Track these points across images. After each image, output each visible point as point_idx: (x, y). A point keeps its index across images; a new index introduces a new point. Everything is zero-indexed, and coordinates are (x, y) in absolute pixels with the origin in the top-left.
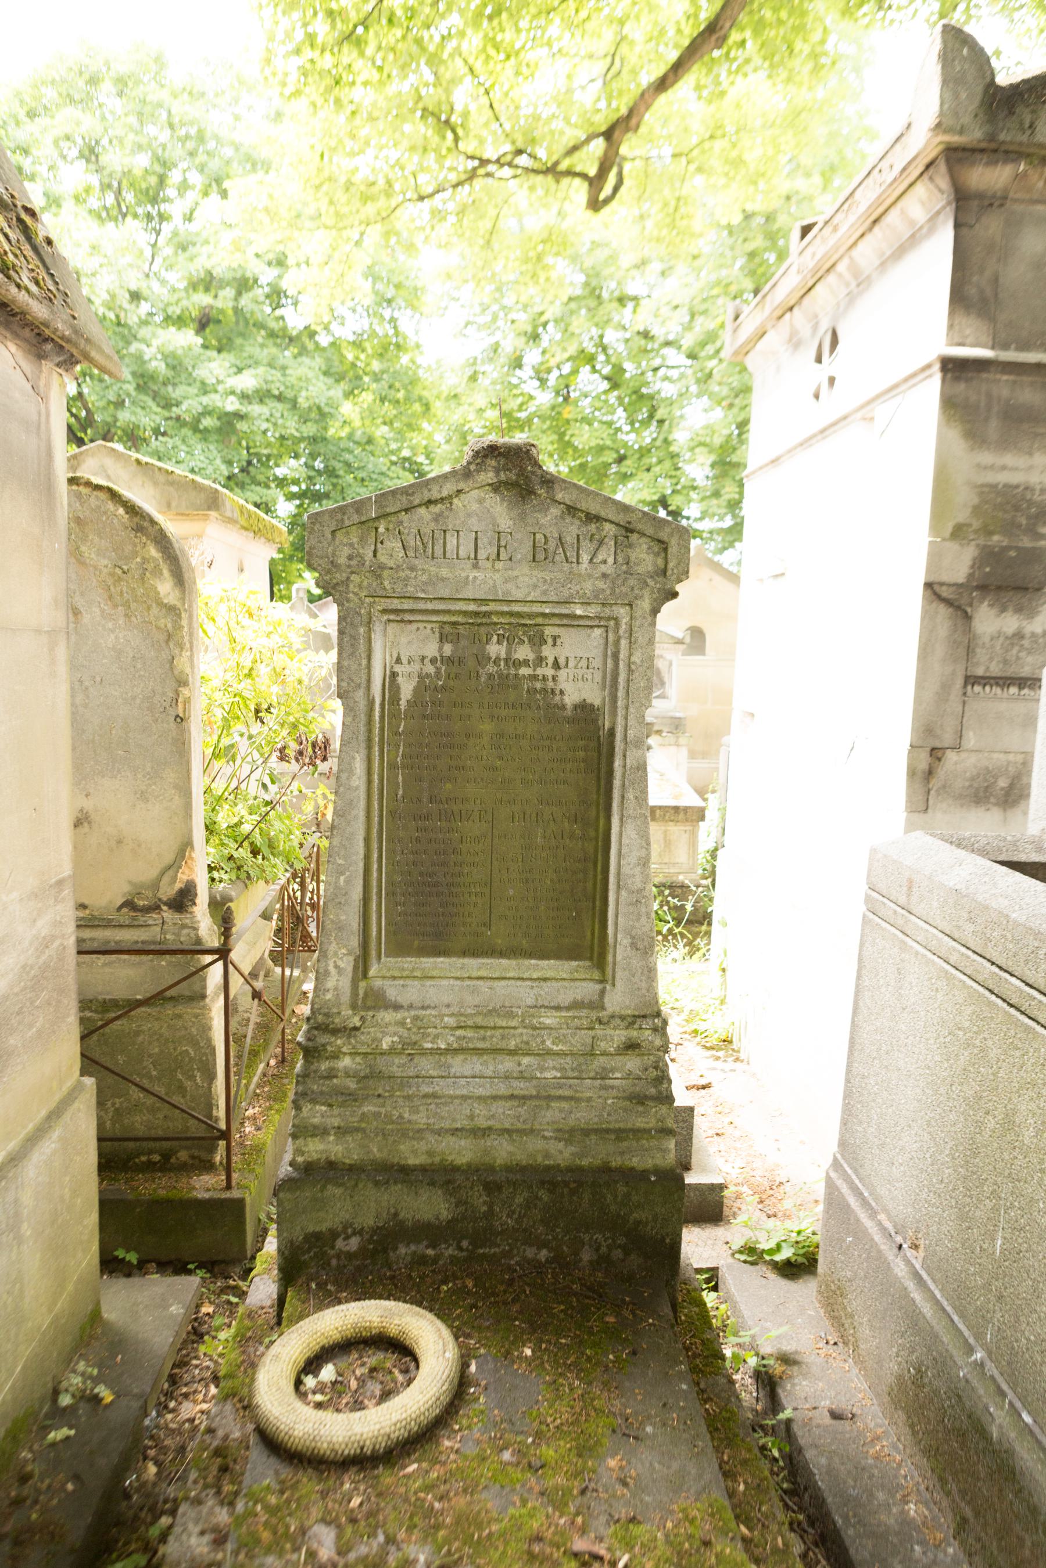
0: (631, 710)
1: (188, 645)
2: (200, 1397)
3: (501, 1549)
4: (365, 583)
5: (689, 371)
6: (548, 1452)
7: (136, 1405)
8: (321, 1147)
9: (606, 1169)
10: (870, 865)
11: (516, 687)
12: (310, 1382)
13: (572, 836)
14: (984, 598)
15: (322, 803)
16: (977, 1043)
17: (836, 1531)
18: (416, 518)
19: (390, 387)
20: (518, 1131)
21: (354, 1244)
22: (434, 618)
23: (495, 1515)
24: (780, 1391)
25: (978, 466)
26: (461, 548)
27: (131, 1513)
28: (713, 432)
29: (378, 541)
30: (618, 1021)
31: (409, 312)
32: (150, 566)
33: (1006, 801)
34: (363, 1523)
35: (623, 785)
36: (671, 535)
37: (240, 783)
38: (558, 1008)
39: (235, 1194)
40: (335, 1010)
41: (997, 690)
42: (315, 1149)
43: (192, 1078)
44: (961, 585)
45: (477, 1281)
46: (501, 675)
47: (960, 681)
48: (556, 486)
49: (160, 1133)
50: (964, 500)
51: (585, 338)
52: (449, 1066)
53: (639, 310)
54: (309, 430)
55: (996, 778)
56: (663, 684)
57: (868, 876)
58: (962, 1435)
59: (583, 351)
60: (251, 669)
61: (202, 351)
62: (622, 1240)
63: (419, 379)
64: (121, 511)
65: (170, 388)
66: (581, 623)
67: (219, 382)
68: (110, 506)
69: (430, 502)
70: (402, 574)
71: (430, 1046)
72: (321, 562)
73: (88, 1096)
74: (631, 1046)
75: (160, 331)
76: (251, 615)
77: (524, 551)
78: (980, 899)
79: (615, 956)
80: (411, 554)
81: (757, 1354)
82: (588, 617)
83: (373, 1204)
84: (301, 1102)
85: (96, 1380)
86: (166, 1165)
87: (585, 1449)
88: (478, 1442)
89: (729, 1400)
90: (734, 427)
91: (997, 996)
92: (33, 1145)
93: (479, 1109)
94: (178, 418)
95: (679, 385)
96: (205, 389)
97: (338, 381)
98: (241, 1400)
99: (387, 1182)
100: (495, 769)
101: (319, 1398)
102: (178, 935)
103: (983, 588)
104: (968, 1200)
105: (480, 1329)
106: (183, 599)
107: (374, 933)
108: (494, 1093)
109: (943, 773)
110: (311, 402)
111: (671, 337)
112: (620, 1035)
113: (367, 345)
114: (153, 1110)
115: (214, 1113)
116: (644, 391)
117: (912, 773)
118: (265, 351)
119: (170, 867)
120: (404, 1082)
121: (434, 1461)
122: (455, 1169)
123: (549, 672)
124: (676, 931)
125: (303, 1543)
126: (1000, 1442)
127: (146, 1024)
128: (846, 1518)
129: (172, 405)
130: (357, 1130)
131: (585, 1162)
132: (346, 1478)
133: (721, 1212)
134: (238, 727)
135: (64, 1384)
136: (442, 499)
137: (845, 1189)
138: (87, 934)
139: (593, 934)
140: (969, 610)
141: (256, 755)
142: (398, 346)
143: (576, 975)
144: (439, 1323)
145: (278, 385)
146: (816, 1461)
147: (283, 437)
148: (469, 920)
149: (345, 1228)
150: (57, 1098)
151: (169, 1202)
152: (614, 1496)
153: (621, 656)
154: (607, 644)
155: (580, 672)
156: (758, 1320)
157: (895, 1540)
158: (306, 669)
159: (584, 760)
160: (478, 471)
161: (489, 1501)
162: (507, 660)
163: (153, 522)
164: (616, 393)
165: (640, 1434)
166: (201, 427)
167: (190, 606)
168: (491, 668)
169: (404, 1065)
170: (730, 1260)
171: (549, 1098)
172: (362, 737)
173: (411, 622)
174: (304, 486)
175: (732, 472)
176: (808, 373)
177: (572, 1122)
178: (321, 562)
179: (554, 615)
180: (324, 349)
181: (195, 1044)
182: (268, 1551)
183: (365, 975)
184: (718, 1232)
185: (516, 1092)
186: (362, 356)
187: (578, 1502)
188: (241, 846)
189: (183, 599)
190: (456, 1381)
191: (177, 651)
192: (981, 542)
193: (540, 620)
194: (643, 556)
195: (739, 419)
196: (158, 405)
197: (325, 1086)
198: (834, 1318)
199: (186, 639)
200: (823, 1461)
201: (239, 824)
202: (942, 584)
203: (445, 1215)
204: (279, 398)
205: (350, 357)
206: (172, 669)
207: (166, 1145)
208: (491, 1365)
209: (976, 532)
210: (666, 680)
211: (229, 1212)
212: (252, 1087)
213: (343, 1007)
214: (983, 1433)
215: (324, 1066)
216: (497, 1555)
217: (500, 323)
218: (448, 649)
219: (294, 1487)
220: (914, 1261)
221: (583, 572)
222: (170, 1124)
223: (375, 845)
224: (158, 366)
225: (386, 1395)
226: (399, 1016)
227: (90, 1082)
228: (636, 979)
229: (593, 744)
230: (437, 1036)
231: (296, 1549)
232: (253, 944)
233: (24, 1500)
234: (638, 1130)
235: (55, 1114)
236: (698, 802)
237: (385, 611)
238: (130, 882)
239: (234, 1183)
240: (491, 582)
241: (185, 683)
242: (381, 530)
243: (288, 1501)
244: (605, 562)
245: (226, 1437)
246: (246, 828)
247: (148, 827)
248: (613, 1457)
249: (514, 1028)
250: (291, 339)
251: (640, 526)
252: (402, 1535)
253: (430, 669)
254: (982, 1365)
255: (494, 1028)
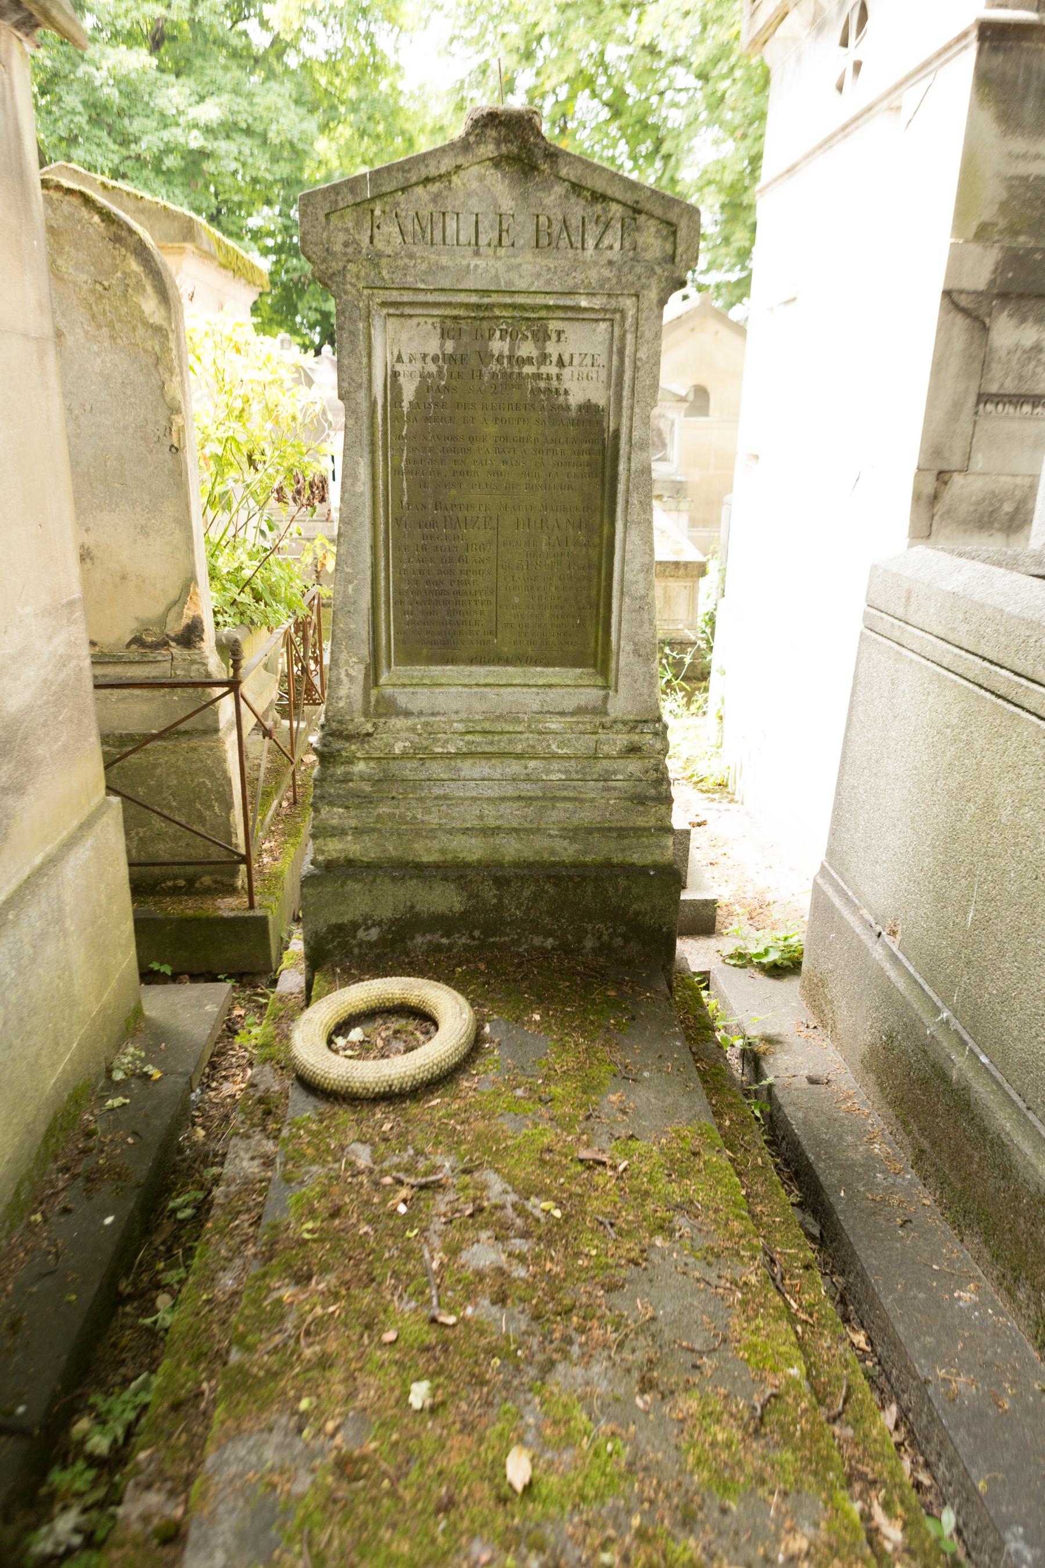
0: (637, 410)
1: (177, 370)
2: (239, 1079)
3: (516, 1157)
4: (363, 273)
5: (699, 95)
6: (557, 1090)
7: (182, 1080)
8: (340, 846)
9: (608, 864)
10: (871, 581)
11: (519, 387)
12: (340, 1041)
13: (576, 543)
14: (1004, 308)
15: (320, 553)
16: (964, 737)
17: (809, 1165)
18: (413, 198)
19: (369, 119)
20: (525, 830)
21: (374, 934)
22: (435, 312)
23: (510, 1134)
24: (763, 1064)
25: (1010, 154)
26: (462, 233)
27: (185, 1165)
28: (724, 168)
29: (375, 226)
30: (621, 726)
31: (387, 26)
32: (132, 282)
33: (1010, 527)
34: (394, 1142)
35: (628, 490)
36: (681, 216)
37: (237, 531)
38: (562, 714)
39: (258, 912)
40: (348, 718)
41: (1010, 409)
42: (335, 848)
43: (210, 807)
44: (981, 293)
45: (489, 964)
46: (504, 374)
47: (972, 399)
48: (560, 160)
49: (183, 859)
50: (993, 192)
51: (583, 55)
52: (459, 770)
53: (644, 18)
54: (283, 169)
55: (1002, 502)
56: (664, 445)
57: (868, 593)
58: (925, 1083)
59: (581, 72)
60: (243, 410)
61: (158, 75)
62: (622, 929)
63: (400, 109)
64: (96, 219)
65: (126, 121)
66: (586, 316)
67: (180, 113)
68: (84, 213)
69: (427, 180)
70: (400, 263)
71: (440, 750)
72: (315, 249)
73: (115, 812)
74: (633, 750)
75: (109, 50)
76: (238, 351)
77: (527, 236)
78: (976, 598)
79: (617, 663)
80: (409, 239)
81: (744, 1037)
82: (593, 309)
83: (390, 899)
84: (320, 805)
85: (145, 1061)
86: (191, 889)
87: (589, 1088)
88: (494, 1083)
89: (717, 1061)
90: (746, 162)
91: (986, 690)
92: (69, 850)
93: (488, 810)
94: (138, 157)
95: (687, 111)
96: (165, 122)
97: (312, 111)
98: (278, 1063)
99: (403, 878)
100: (499, 474)
101: (349, 1053)
102: (188, 671)
103: (1004, 296)
104: (945, 882)
105: (492, 1000)
106: (169, 318)
107: (383, 642)
108: (502, 794)
109: (948, 498)
110: (283, 137)
111: (680, 53)
112: (622, 740)
113: (342, 68)
114: (175, 839)
115: (234, 840)
116: (650, 121)
117: (917, 497)
118: (229, 75)
119: (175, 603)
120: (417, 784)
121: (455, 1098)
122: (467, 865)
123: (553, 370)
124: (675, 683)
125: (343, 1156)
126: (958, 1082)
127: (163, 757)
128: (818, 1155)
129: (130, 142)
130: (373, 830)
131: (588, 859)
132: (377, 1110)
133: (714, 925)
134: (232, 473)
135: (116, 1063)
136: (440, 176)
137: (830, 892)
138: (100, 670)
139: (596, 642)
140: (987, 321)
141: (252, 503)
142: (376, 68)
143: (580, 682)
144: (455, 993)
145: (245, 116)
146: (794, 1116)
147: (255, 181)
148: (476, 628)
149: (365, 920)
150: (87, 811)
151: (197, 919)
152: (615, 1121)
153: (627, 352)
154: (612, 339)
155: (585, 370)
156: (745, 1010)
157: (861, 1170)
158: (299, 405)
159: (589, 464)
160: (478, 143)
161: (505, 1124)
162: (510, 358)
163: (131, 231)
164: (617, 123)
165: (638, 1077)
166: (164, 168)
167: (177, 327)
168: (494, 367)
169: (415, 769)
170: (721, 965)
171: (554, 799)
172: (366, 441)
173: (411, 316)
174: (279, 239)
175: (743, 215)
176: (829, 58)
177: (576, 821)
178: (315, 249)
179: (558, 307)
180: (294, 73)
181: (211, 776)
182: (313, 1162)
183: (376, 684)
184: (710, 944)
185: (523, 794)
186: (337, 81)
187: (583, 1125)
188: (242, 591)
189: (169, 319)
190: (473, 1037)
191: (167, 376)
192: (1006, 243)
193: (543, 314)
194: (651, 240)
195: (753, 152)
196: (115, 142)
197: (341, 789)
198: (814, 1007)
199: (176, 363)
200: (800, 1115)
201: (241, 568)
202: (961, 292)
203: (458, 907)
204: (248, 132)
205: (323, 81)
206: (163, 396)
207: (190, 869)
208: (503, 1027)
209: (1001, 232)
210: (668, 441)
211: (254, 930)
212: (268, 819)
213: (356, 715)
214: (943, 1076)
215: (340, 770)
216: (513, 1161)
217: (490, 37)
218: (450, 346)
219: (332, 1117)
220: (891, 945)
221: (589, 259)
222: (193, 852)
223: (381, 553)
224: (111, 93)
225: (409, 1049)
226: (410, 722)
227: (116, 800)
228: (638, 685)
229: (597, 447)
230: (447, 741)
231: (337, 1160)
232: (262, 690)
233: (91, 1150)
234: (639, 829)
235: (87, 825)
236: (698, 557)
237: (384, 304)
238: (137, 619)
239: (256, 904)
240: (493, 271)
241: (178, 411)
242: (377, 212)
243: (327, 1127)
244: (611, 247)
245: (267, 1090)
246: (247, 573)
247: (150, 562)
248: (614, 1093)
249: (521, 733)
250: (257, 61)
251: (648, 207)
252: (429, 1149)
253: (432, 368)
254: (947, 1022)
255: (502, 733)
